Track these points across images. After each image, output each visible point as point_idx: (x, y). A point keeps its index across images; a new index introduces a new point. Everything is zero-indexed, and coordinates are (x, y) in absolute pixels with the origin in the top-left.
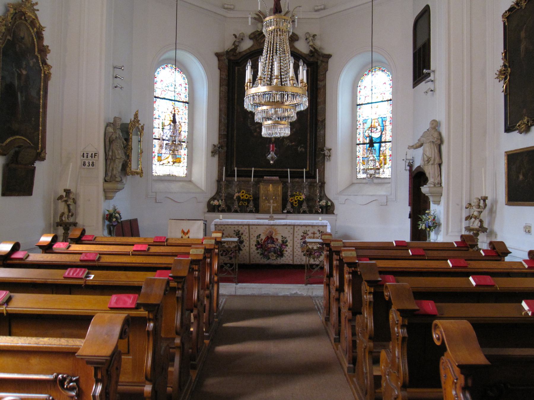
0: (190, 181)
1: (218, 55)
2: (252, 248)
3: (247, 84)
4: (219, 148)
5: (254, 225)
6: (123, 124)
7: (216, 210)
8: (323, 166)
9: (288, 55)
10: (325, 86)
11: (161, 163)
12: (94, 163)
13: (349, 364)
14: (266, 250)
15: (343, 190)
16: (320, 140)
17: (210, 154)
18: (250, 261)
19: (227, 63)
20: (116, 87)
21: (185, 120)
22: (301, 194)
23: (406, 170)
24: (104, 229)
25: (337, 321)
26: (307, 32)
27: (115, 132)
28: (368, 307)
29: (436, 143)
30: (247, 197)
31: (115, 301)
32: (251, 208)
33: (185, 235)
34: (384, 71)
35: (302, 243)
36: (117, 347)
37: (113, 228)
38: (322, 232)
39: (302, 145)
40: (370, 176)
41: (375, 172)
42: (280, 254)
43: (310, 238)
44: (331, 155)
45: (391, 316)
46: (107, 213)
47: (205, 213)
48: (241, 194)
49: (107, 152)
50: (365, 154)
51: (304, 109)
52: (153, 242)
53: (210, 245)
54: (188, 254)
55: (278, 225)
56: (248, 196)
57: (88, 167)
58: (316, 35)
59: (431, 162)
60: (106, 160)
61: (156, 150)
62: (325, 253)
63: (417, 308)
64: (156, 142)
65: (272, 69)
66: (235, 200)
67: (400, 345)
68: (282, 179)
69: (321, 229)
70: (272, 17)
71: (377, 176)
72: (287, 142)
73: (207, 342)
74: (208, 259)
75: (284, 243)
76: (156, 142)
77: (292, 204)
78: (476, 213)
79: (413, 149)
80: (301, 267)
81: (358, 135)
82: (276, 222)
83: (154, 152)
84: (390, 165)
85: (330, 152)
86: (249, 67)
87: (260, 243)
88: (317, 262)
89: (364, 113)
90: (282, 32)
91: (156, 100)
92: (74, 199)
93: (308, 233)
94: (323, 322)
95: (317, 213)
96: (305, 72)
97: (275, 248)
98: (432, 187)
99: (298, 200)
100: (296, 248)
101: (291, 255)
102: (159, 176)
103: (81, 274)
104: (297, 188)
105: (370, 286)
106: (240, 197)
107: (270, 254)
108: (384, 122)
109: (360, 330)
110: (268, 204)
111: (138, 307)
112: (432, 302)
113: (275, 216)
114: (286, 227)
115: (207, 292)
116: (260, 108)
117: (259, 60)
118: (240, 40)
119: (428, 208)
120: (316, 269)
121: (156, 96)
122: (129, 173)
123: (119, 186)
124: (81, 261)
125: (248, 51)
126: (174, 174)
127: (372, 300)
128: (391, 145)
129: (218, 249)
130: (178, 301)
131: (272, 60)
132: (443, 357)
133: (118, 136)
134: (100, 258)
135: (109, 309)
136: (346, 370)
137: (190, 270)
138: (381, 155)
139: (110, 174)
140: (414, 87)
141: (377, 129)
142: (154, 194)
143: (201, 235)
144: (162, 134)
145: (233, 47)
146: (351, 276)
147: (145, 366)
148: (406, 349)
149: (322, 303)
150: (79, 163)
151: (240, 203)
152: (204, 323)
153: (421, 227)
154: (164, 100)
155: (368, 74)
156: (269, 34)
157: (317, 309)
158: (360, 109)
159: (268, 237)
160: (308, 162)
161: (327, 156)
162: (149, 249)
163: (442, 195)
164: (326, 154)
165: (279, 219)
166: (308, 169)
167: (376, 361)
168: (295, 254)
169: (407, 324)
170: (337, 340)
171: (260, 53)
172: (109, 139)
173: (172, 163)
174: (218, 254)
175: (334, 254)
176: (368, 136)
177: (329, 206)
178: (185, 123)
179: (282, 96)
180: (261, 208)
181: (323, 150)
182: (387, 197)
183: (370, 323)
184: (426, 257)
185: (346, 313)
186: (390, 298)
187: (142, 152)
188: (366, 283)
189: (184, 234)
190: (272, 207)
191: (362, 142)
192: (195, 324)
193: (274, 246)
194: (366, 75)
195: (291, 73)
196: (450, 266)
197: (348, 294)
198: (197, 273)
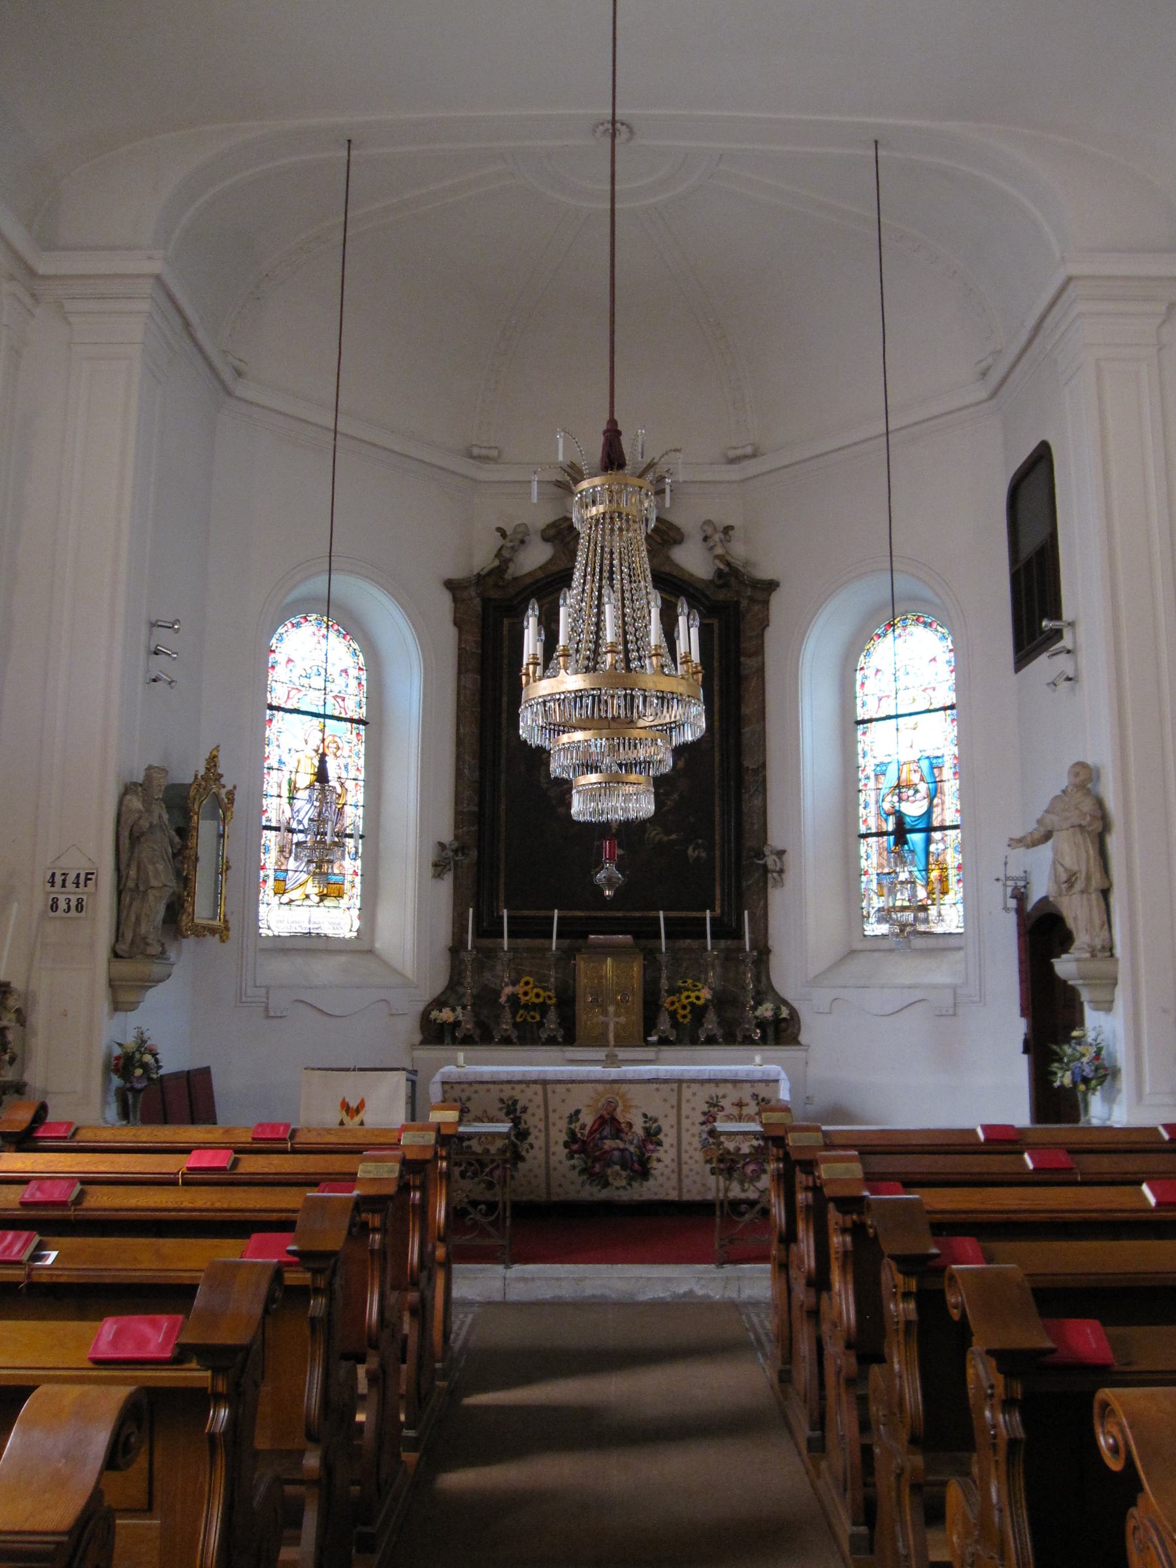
0: (371, 952)
1: (451, 585)
2: (554, 1154)
3: (527, 669)
4: (456, 851)
5: (559, 1082)
6: (172, 787)
7: (448, 1039)
8: (762, 902)
9: (646, 584)
10: (761, 671)
11: (285, 899)
12: (84, 903)
13: (854, 1523)
14: (596, 1160)
15: (824, 973)
16: (752, 824)
17: (429, 870)
18: (549, 1193)
19: (479, 609)
20: (154, 680)
21: (358, 773)
22: (700, 985)
23: (1006, 909)
24: (105, 1103)
25: (816, 1382)
26: (703, 519)
27: (149, 810)
28: (901, 1335)
29: (1090, 829)
31: (111, 1336)
32: (552, 1030)
33: (352, 1118)
34: (931, 625)
35: (704, 1136)
36: (97, 1495)
37: (135, 1097)
40: (902, 931)
41: (916, 918)
42: (641, 1169)
43: (730, 1118)
44: (785, 868)
45: (970, 1371)
46: (117, 1051)
47: (413, 1047)
48: (520, 989)
49: (123, 867)
51: (695, 739)
52: (250, 1140)
53: (424, 1148)
54: (350, 1178)
55: (631, 1082)
57: (65, 915)
59: (1079, 886)
60: (120, 893)
61: (270, 859)
62: (772, 1167)
63: (1049, 1344)
64: (270, 837)
65: (599, 625)
66: (504, 1007)
67: (1003, 1466)
68: (643, 942)
69: (763, 1091)
70: (597, 481)
71: (922, 928)
72: (654, 833)
73: (410, 1457)
74: (414, 1191)
75: (652, 1135)
76: (270, 837)
77: (673, 1015)
79: (1022, 849)
80: (703, 1209)
81: (861, 808)
82: (625, 1071)
83: (263, 868)
84: (961, 895)
85: (780, 858)
86: (531, 619)
87: (579, 1135)
88: (752, 1195)
90: (627, 521)
91: (273, 715)
92: (18, 1011)
93: (723, 1103)
94: (772, 1387)
95: (748, 1041)
96: (694, 632)
97: (623, 1150)
98: (1085, 960)
99: (692, 1004)
100: (686, 1152)
101: (673, 1171)
102: (279, 936)
103: (16, 1249)
104: (687, 968)
105: (906, 1274)
106: (519, 998)
107: (609, 1171)
108: (935, 770)
109: (880, 1413)
110: (602, 1018)
111: (182, 1355)
112: (1096, 1323)
113: (623, 1054)
114: (655, 1086)
115: (413, 1296)
116: (565, 738)
117: (561, 602)
118: (517, 543)
119: (1079, 1022)
120: (747, 1217)
121: (274, 704)
122: (187, 930)
123: (156, 969)
124: (25, 1204)
125: (541, 575)
126: (321, 931)
127: (914, 1317)
128: (960, 836)
129: (447, 1158)
130: (313, 1330)
131: (600, 597)
132: (1133, 1511)
133: (155, 821)
134: (82, 1194)
135: (90, 1365)
136: (846, 1547)
137: (354, 1230)
138: (933, 866)
139: (129, 935)
140: (1017, 670)
141: (917, 791)
142: (263, 991)
143: (399, 1116)
144: (288, 814)
145: (497, 563)
146: (848, 1239)
147: (200, 1552)
148: (1021, 1483)
149: (767, 1324)
150: (40, 902)
152: (402, 1396)
153: (1062, 1082)
154: (295, 715)
155: (885, 635)
156: (591, 528)
157: (755, 1344)
159: (601, 1117)
161: (773, 871)
162: (236, 1163)
163: (1115, 984)
164: (770, 866)
166: (718, 910)
167: (934, 1515)
168: (685, 1168)
169: (1019, 1397)
170: (817, 1446)
171: (564, 579)
172: (131, 831)
173: (317, 899)
174: (447, 1176)
175: (797, 1169)
176: (892, 810)
177: (784, 1019)
178: (354, 782)
179: (630, 701)
180: (580, 1032)
181: (760, 854)
183: (912, 1392)
184: (1076, 1174)
185: (838, 1357)
186: (964, 1315)
187: (227, 869)
188: (893, 1264)
189: (347, 1113)
190: (612, 1027)
191: (874, 830)
192: (374, 1399)
193: (622, 1145)
194: (879, 636)
195: (655, 635)
196: (1149, 1203)
197: (843, 1296)
198: (378, 1237)
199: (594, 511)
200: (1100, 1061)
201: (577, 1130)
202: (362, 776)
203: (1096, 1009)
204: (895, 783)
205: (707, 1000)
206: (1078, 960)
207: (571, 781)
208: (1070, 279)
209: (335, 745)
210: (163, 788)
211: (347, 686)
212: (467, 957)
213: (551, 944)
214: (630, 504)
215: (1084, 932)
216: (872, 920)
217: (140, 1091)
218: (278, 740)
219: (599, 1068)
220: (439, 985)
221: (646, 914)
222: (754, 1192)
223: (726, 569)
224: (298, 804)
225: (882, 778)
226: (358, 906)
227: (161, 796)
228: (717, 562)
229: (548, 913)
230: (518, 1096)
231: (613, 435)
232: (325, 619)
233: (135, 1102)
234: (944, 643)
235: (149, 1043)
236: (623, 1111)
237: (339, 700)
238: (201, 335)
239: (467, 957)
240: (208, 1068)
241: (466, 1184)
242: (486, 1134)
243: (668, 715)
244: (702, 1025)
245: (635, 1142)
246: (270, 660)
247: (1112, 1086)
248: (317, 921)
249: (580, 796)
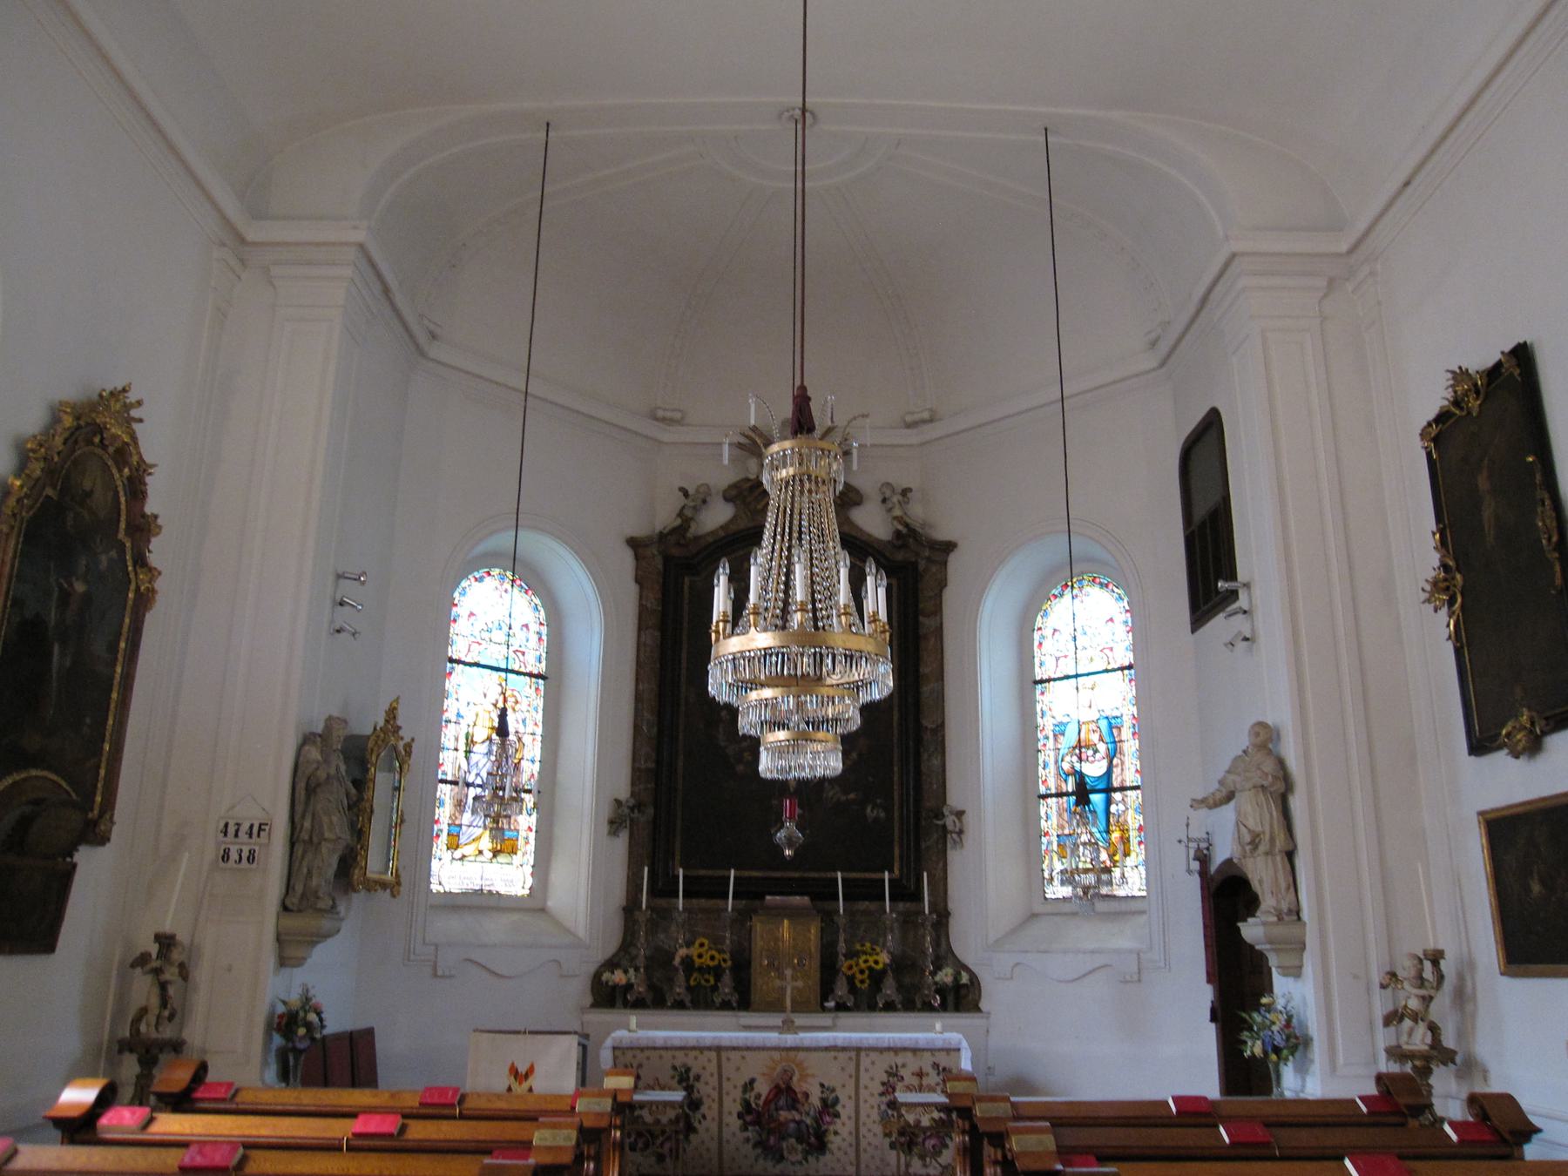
1: (633, 543)
3: (717, 626)
4: (632, 809)
5: (734, 1049)
7: (619, 1002)
8: (941, 865)
9: (834, 545)
10: (939, 630)
11: (458, 854)
12: (256, 855)
17: (605, 828)
19: (660, 567)
20: (338, 631)
21: (535, 728)
22: (878, 949)
24: (265, 1063)
27: (326, 761)
30: (712, 958)
32: (726, 994)
33: (520, 1083)
34: (1107, 586)
35: (883, 1107)
37: (296, 1060)
40: (1085, 893)
41: (1099, 881)
43: (909, 1089)
44: (965, 829)
46: (281, 1009)
47: (583, 1010)
48: (694, 951)
49: (296, 820)
53: (600, 1115)
54: (525, 1146)
57: (235, 866)
58: (910, 490)
59: (1262, 848)
61: (444, 814)
64: (445, 791)
65: (788, 585)
66: (676, 969)
69: (943, 1061)
70: (787, 444)
71: (1104, 890)
72: (831, 794)
75: (829, 1107)
77: (851, 980)
78: (1414, 1004)
81: (1040, 768)
84: (1142, 858)
85: (959, 819)
87: (754, 1105)
90: (817, 483)
92: (182, 966)
93: (902, 1072)
95: (928, 1007)
96: (882, 592)
97: (798, 1123)
98: (1272, 923)
99: (870, 968)
107: (784, 1145)
110: (778, 983)
113: (800, 1020)
114: (833, 1054)
116: (754, 695)
117: (752, 561)
123: (326, 924)
125: (722, 534)
126: (494, 889)
128: (1140, 796)
129: (622, 1128)
131: (789, 558)
133: (333, 771)
134: (244, 1159)
139: (299, 888)
140: (1193, 631)
141: (1096, 751)
143: (569, 1084)
144: (464, 766)
145: (679, 521)
150: (211, 853)
151: (692, 979)
155: (1062, 595)
160: (897, 851)
161: (951, 832)
162: (403, 1129)
164: (950, 827)
166: (897, 872)
171: (754, 538)
173: (491, 855)
174: (620, 1146)
175: (985, 1142)
177: (965, 985)
178: (531, 737)
179: (818, 660)
180: (755, 997)
187: (402, 821)
191: (1053, 791)
193: (797, 1117)
194: (1055, 597)
195: (843, 595)
199: (784, 473)
200: (1291, 1030)
201: (752, 1100)
202: (539, 731)
203: (1285, 975)
204: (1074, 742)
205: (885, 964)
206: (1264, 924)
207: (759, 738)
208: (1234, 256)
210: (342, 738)
211: (527, 640)
212: (642, 917)
213: (727, 904)
214: (818, 468)
215: (1270, 895)
216: (1056, 882)
217: (301, 1051)
218: (457, 693)
220: (609, 944)
221: (823, 875)
222: (935, 1168)
223: (904, 531)
224: (474, 758)
226: (532, 863)
227: (339, 747)
228: (895, 523)
229: (726, 873)
230: (690, 1062)
231: (802, 401)
232: (509, 574)
233: (296, 1066)
234: (1121, 604)
235: (314, 1001)
236: (799, 1080)
237: (519, 654)
238: (399, 299)
239: (642, 917)
240: (373, 1029)
241: (637, 1157)
242: (657, 1103)
243: (856, 674)
244: (879, 990)
245: (812, 1113)
246: (453, 614)
247: (1305, 1055)
249: (768, 753)
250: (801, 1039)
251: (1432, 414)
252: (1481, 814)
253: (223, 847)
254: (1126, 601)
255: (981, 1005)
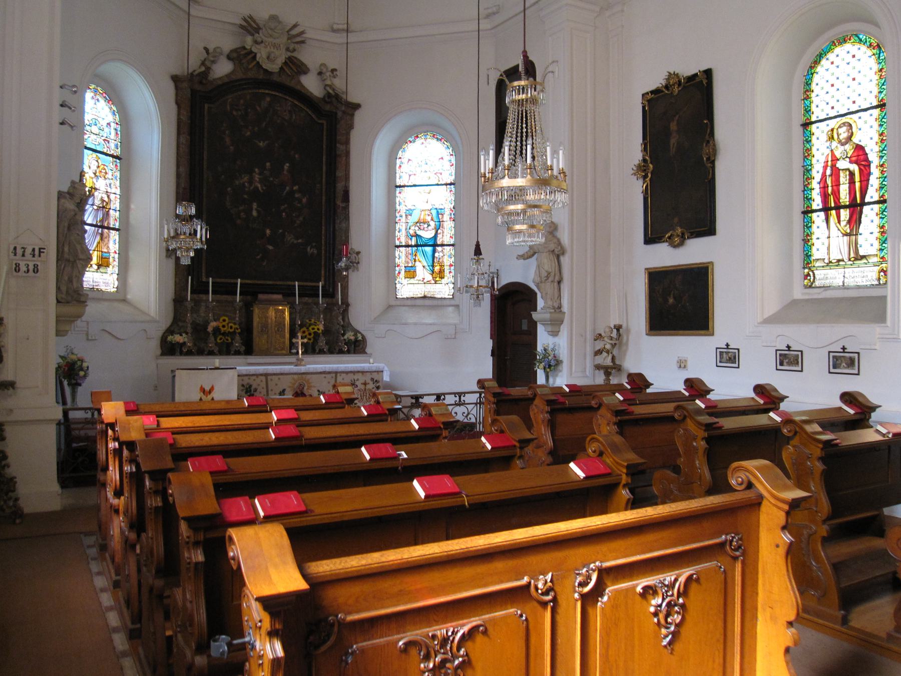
0: (124, 300)
5: (274, 374)
10: (348, 154)
12: (39, 267)
21: (116, 190)
26: (320, 63)
30: (231, 327)
33: (207, 396)
34: (441, 140)
38: (376, 381)
39: (314, 244)
47: (157, 358)
50: (410, 262)
56: (234, 326)
57: (25, 274)
59: (550, 279)
66: (209, 334)
72: (289, 239)
78: (608, 347)
81: (397, 232)
89: (407, 199)
93: (357, 383)
95: (341, 352)
99: (315, 333)
112: (296, 492)
114: (324, 375)
125: (226, 80)
141: (429, 225)
145: (203, 69)
151: (219, 338)
155: (414, 142)
158: (400, 193)
160: (323, 272)
165: (267, 363)
176: (414, 234)
178: (114, 195)
180: (255, 348)
182: (455, 325)
189: (204, 394)
191: (404, 244)
194: (410, 142)
202: (118, 192)
209: (104, 171)
213: (209, 297)
219: (292, 367)
225: (409, 217)
228: (328, 88)
234: (448, 150)
236: (308, 389)
248: (96, 280)
250: (309, 368)
251: (653, 87)
252: (646, 269)
253: (14, 262)
254: (451, 149)
255: (366, 350)
